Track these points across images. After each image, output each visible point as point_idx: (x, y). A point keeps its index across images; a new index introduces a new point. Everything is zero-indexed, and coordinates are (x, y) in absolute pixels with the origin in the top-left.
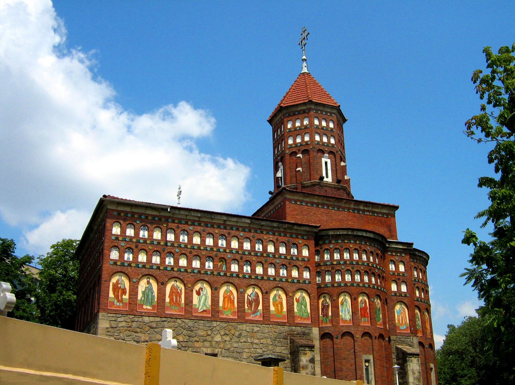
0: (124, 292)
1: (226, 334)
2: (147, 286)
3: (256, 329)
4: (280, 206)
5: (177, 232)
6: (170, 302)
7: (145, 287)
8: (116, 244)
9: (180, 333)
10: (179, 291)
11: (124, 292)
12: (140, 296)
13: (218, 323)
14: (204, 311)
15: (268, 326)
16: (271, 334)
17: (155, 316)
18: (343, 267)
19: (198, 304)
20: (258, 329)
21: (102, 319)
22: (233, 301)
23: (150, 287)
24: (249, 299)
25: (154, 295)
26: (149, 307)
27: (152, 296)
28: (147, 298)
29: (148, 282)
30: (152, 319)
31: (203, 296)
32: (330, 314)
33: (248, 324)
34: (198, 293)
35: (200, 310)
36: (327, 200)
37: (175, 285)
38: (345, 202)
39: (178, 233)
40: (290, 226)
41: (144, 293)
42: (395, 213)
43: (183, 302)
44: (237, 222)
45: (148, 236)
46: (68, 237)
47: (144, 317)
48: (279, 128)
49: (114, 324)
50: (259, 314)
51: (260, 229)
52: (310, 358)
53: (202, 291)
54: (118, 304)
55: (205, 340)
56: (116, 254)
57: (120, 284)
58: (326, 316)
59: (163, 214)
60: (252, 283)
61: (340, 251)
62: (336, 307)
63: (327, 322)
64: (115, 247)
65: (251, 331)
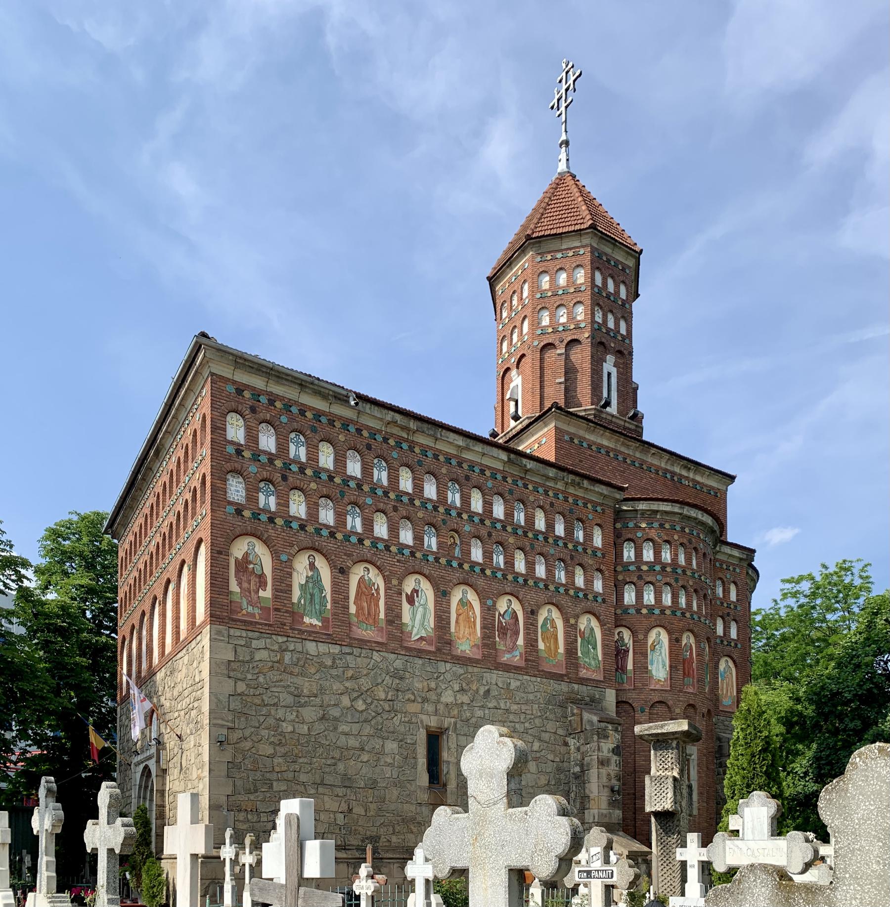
0: (262, 581)
1: (462, 690)
2: (310, 574)
3: (514, 684)
4: (537, 445)
5: (369, 458)
6: (357, 615)
7: (305, 575)
8: (238, 466)
9: (380, 681)
10: (374, 591)
11: (262, 584)
12: (296, 594)
13: (448, 666)
14: (422, 638)
15: (533, 679)
16: (538, 694)
17: (331, 640)
18: (659, 577)
19: (410, 623)
20: (518, 683)
21: (216, 639)
22: (474, 622)
23: (316, 576)
24: (502, 623)
25: (325, 596)
26: (315, 622)
27: (321, 597)
28: (311, 601)
29: (312, 566)
30: (323, 648)
31: (418, 607)
32: (630, 666)
33: (500, 673)
34: (411, 600)
35: (416, 635)
36: (623, 444)
37: (366, 578)
38: (654, 454)
39: (369, 461)
40: (577, 479)
41: (303, 587)
42: (727, 491)
43: (382, 616)
44: (484, 454)
45: (309, 459)
46: (87, 509)
47: (307, 642)
48: (514, 292)
49: (244, 655)
50: (517, 653)
51: (522, 478)
52: (613, 746)
53: (417, 596)
54: (250, 609)
55: (425, 700)
56: (238, 491)
57: (251, 563)
58: (622, 670)
59: (338, 410)
60: (508, 590)
61: (654, 545)
62: (642, 653)
63: (623, 683)
64: (238, 472)
65: (505, 687)
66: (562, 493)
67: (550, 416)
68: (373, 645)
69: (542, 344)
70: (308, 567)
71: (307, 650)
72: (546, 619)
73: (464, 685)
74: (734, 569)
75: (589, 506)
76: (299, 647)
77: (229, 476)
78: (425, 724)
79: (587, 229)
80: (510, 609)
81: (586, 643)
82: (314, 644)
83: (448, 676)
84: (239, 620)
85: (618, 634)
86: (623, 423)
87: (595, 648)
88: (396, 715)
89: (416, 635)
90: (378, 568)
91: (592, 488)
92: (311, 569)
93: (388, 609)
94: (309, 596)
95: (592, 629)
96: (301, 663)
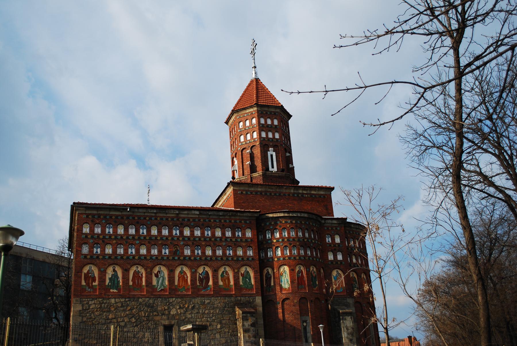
2: (113, 273)
3: (207, 301)
9: (142, 309)
11: (94, 280)
12: (107, 281)
14: (162, 290)
18: (281, 244)
22: (187, 279)
25: (119, 280)
26: (115, 291)
27: (117, 281)
29: (114, 270)
34: (157, 276)
37: (137, 270)
41: (110, 279)
43: (144, 284)
53: (160, 274)
54: (89, 290)
56: (86, 249)
57: (90, 273)
66: (228, 220)
67: (231, 186)
68: (139, 296)
69: (242, 149)
70: (112, 271)
71: (111, 302)
72: (223, 272)
73: (182, 306)
74: (336, 229)
75: (243, 222)
76: (108, 301)
77: (83, 245)
78: (163, 324)
79: (254, 105)
80: (205, 271)
81: (245, 279)
82: (114, 299)
83: (174, 303)
84: (84, 295)
85: (267, 270)
86: (278, 175)
87: (250, 279)
88: (149, 322)
89: (159, 289)
90: (142, 266)
91: (242, 215)
92: (113, 272)
93: (146, 281)
94: (112, 282)
95: (248, 272)
96: (108, 307)
